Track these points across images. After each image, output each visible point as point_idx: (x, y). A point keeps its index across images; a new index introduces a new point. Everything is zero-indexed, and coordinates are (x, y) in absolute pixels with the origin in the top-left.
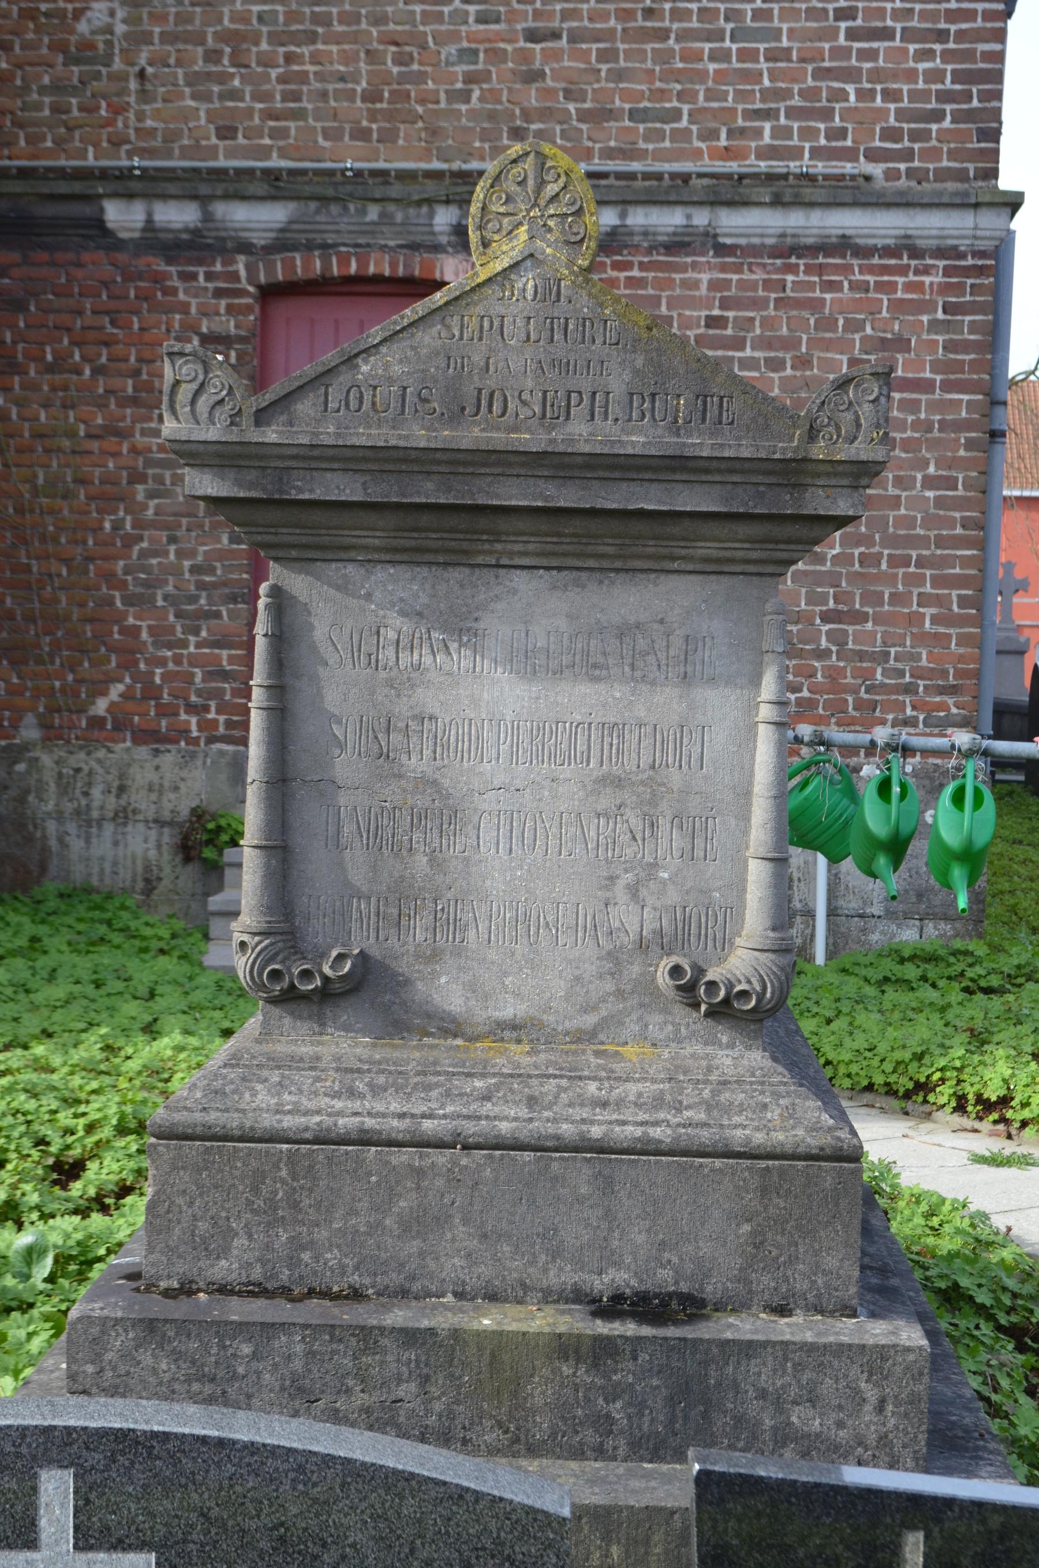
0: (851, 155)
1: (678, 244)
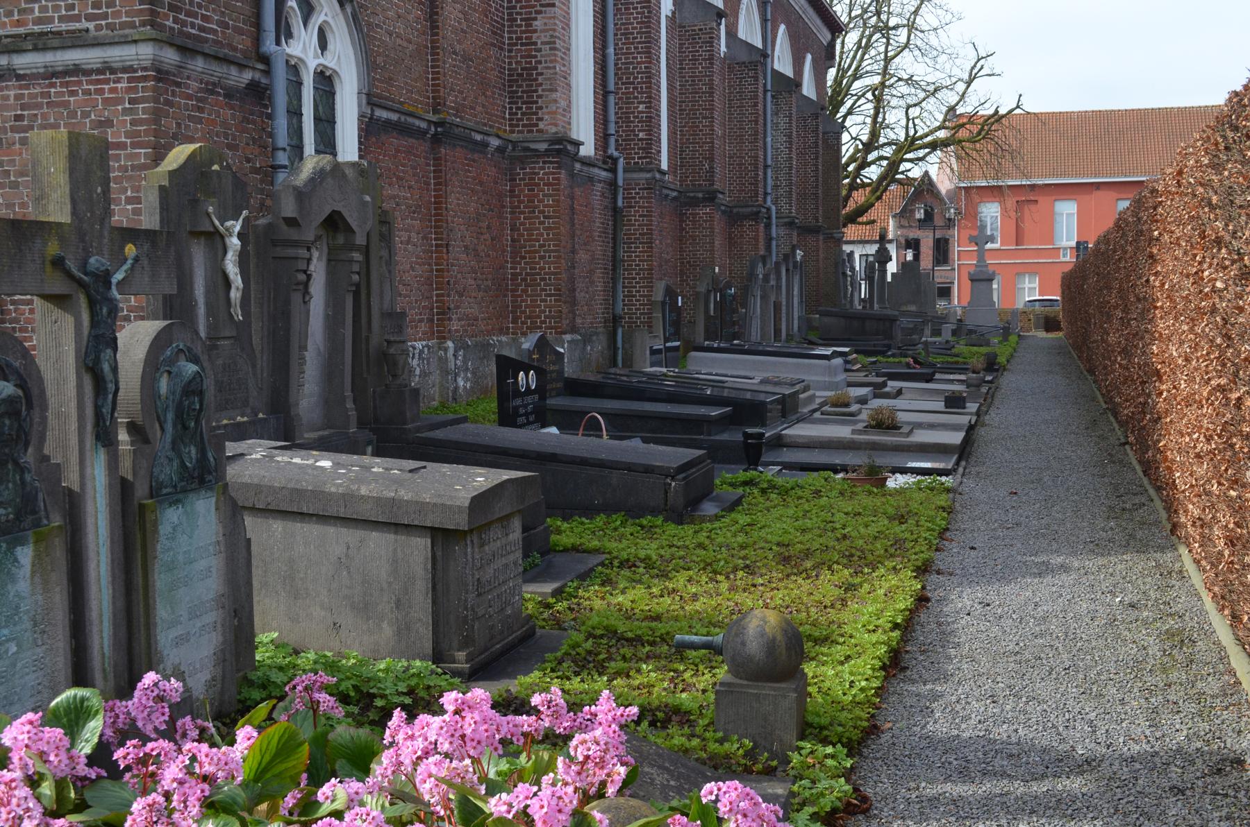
0: (77, 18)
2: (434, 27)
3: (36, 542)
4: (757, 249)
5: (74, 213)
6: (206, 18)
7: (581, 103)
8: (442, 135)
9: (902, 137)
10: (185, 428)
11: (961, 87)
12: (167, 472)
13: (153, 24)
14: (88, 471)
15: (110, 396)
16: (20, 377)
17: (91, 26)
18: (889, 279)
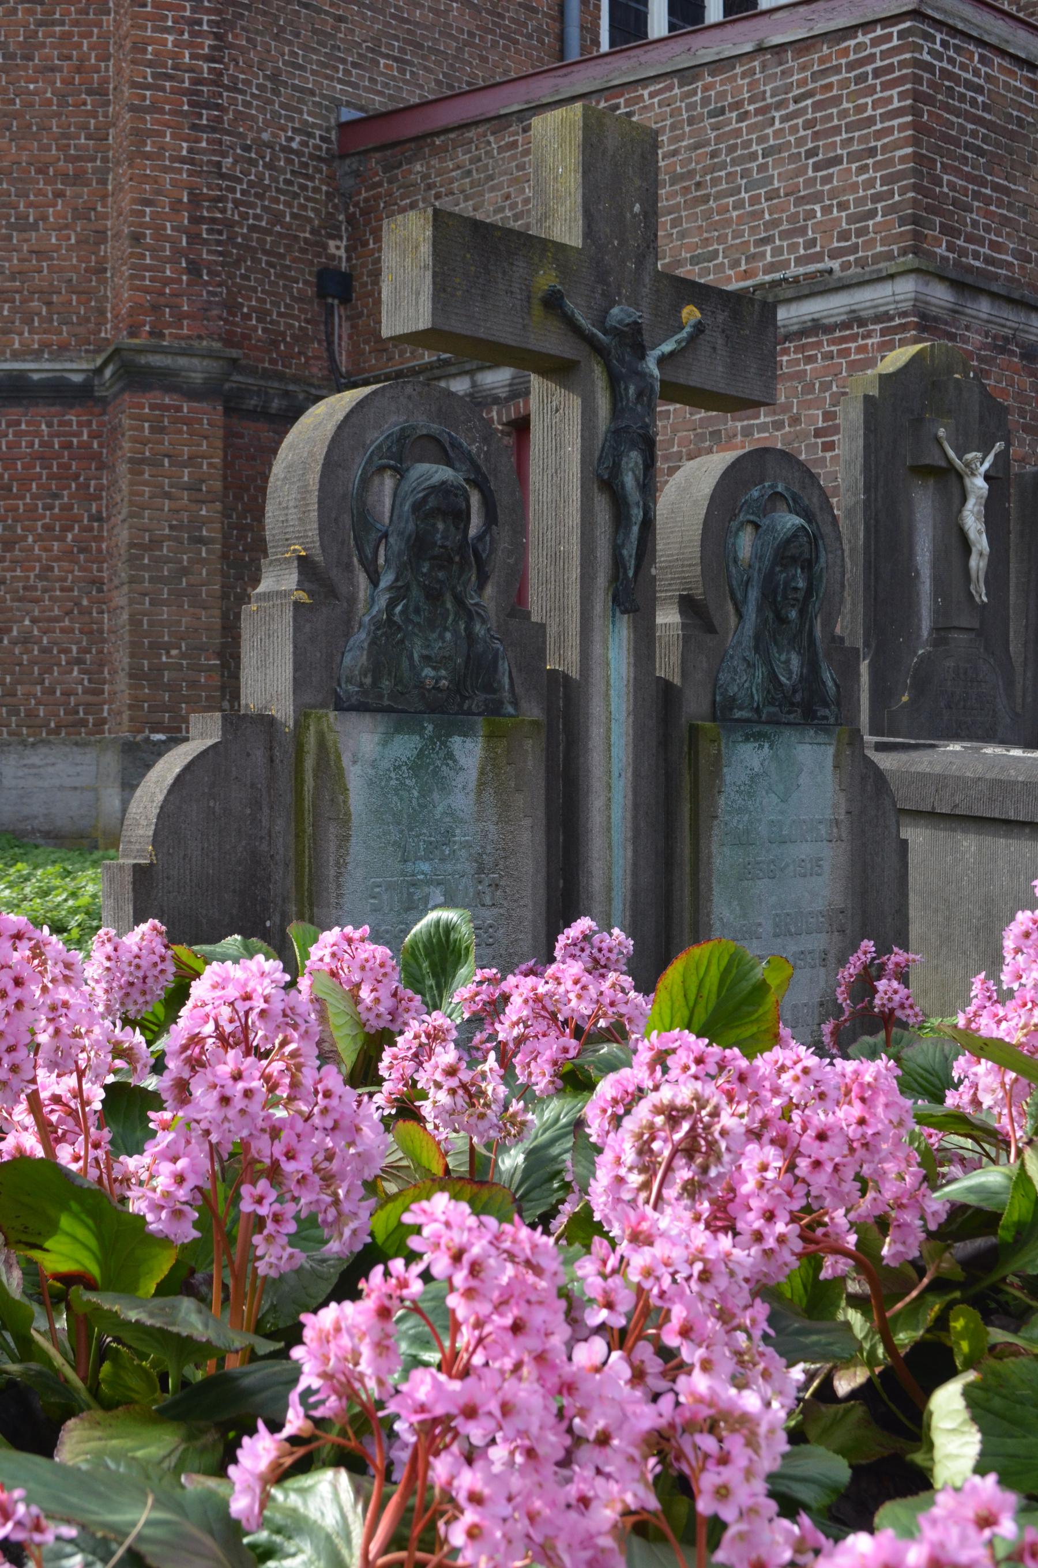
0: (818, 258)
3: (490, 737)
5: (589, 233)
6: (995, 246)
10: (781, 619)
12: (745, 682)
13: (916, 251)
14: (597, 649)
15: (635, 529)
16: (476, 467)
17: (835, 265)
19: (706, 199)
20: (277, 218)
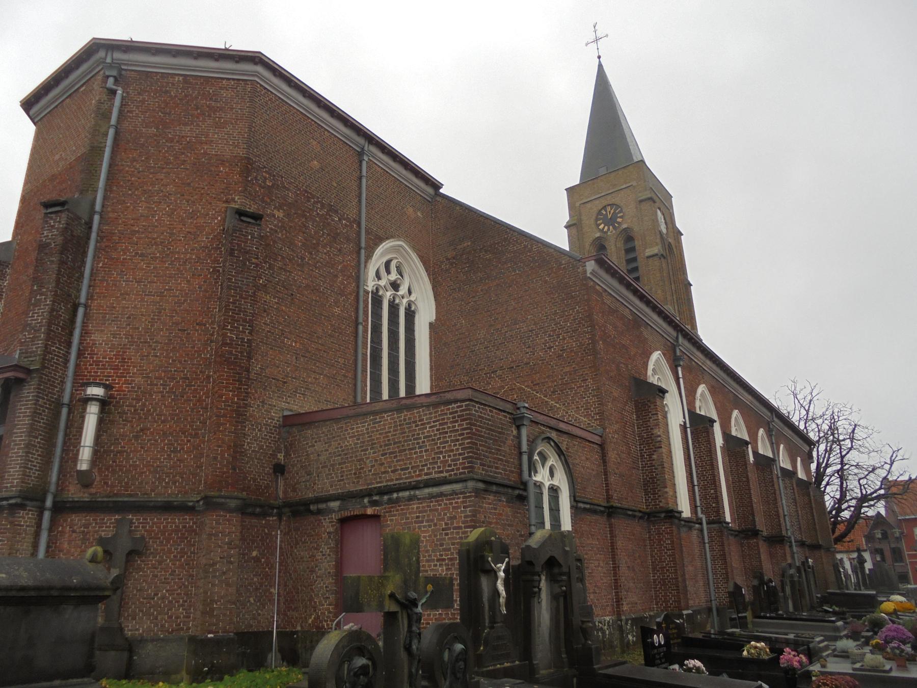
0: (441, 472)
1: (410, 499)
2: (604, 462)
4: (786, 560)
6: (497, 468)
7: (682, 492)
8: (611, 511)
9: (859, 495)
11: (887, 467)
17: (447, 474)
18: (867, 572)
19: (405, 450)
20: (261, 447)
